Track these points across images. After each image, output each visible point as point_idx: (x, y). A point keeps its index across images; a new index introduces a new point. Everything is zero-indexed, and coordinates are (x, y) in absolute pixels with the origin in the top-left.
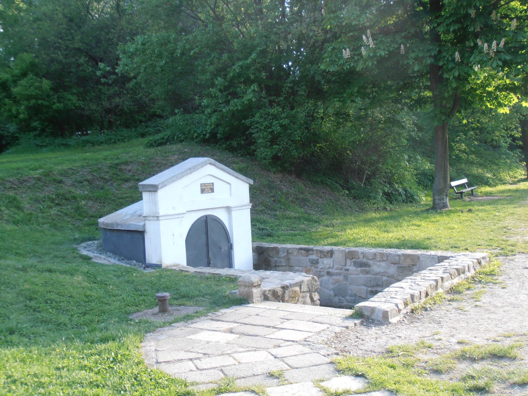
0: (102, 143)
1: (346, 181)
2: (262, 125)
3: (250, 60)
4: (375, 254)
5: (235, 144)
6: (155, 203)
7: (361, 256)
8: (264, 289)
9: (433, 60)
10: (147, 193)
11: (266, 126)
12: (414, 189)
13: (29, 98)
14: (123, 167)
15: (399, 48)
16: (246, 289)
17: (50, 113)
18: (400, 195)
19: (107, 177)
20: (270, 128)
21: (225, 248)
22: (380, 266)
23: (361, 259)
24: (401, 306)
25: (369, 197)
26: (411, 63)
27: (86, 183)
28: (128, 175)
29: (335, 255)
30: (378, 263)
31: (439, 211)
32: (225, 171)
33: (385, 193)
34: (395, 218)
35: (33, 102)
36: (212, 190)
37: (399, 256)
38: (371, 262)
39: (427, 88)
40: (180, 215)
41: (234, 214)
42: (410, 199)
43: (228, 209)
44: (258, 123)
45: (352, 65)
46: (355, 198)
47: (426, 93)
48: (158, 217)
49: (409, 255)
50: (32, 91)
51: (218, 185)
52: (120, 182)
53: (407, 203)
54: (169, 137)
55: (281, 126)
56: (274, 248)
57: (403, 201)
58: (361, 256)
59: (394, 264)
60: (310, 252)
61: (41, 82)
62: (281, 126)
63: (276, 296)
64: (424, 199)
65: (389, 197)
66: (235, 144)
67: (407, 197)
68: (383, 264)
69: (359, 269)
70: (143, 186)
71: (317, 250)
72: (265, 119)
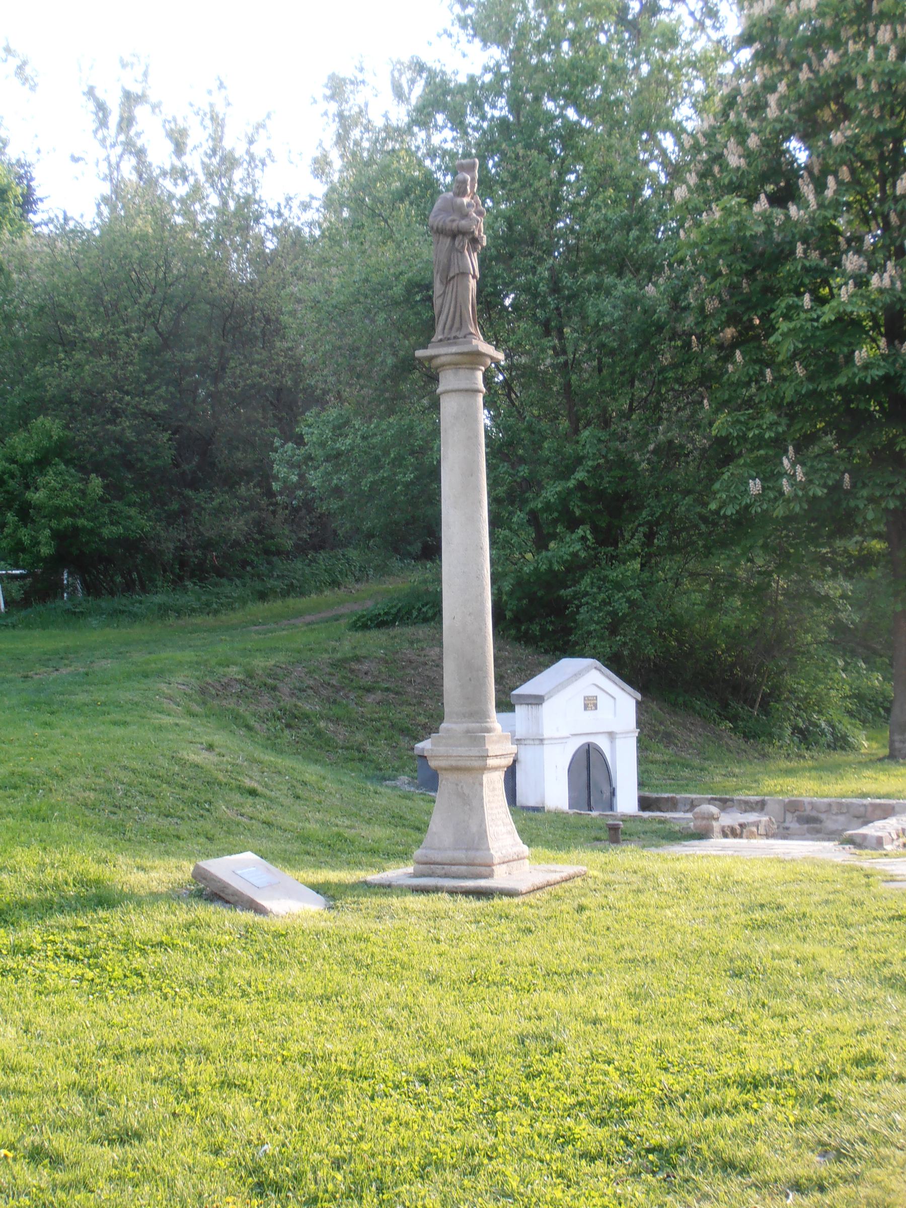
0: (193, 610)
1: (725, 705)
2: (595, 600)
3: (573, 481)
4: (830, 805)
5: (536, 629)
6: (538, 721)
7: (808, 808)
8: (723, 824)
9: (898, 503)
10: (524, 707)
11: (603, 601)
12: (846, 726)
13: (58, 512)
14: (354, 666)
15: (842, 479)
16: (704, 822)
17: (94, 546)
18: (822, 731)
19: (334, 682)
20: (610, 603)
21: (607, 794)
22: (836, 821)
23: (808, 812)
24: (895, 837)
25: (771, 735)
26: (861, 506)
27: (310, 692)
28: (367, 681)
29: (769, 807)
30: (834, 817)
31: (901, 761)
32: (610, 679)
33: (796, 729)
34: (835, 769)
35: (67, 521)
36: (596, 707)
37: (865, 805)
38: (823, 816)
39: (878, 536)
40: (563, 739)
41: (619, 742)
42: (841, 743)
43: (611, 735)
44: (586, 594)
45: (765, 506)
46: (746, 737)
47: (878, 546)
48: (542, 740)
49: (880, 805)
50: (66, 500)
51: (602, 700)
52: (360, 692)
53: (835, 749)
54: (399, 611)
55: (629, 600)
56: (668, 799)
57: (829, 746)
58: (808, 808)
59: (858, 817)
60: (729, 803)
61: (86, 481)
62: (629, 600)
63: (732, 832)
64: (866, 744)
65: (806, 737)
66: (536, 629)
67: (836, 739)
68: (841, 818)
69: (806, 826)
70: (519, 696)
71: (740, 800)
72: (599, 588)
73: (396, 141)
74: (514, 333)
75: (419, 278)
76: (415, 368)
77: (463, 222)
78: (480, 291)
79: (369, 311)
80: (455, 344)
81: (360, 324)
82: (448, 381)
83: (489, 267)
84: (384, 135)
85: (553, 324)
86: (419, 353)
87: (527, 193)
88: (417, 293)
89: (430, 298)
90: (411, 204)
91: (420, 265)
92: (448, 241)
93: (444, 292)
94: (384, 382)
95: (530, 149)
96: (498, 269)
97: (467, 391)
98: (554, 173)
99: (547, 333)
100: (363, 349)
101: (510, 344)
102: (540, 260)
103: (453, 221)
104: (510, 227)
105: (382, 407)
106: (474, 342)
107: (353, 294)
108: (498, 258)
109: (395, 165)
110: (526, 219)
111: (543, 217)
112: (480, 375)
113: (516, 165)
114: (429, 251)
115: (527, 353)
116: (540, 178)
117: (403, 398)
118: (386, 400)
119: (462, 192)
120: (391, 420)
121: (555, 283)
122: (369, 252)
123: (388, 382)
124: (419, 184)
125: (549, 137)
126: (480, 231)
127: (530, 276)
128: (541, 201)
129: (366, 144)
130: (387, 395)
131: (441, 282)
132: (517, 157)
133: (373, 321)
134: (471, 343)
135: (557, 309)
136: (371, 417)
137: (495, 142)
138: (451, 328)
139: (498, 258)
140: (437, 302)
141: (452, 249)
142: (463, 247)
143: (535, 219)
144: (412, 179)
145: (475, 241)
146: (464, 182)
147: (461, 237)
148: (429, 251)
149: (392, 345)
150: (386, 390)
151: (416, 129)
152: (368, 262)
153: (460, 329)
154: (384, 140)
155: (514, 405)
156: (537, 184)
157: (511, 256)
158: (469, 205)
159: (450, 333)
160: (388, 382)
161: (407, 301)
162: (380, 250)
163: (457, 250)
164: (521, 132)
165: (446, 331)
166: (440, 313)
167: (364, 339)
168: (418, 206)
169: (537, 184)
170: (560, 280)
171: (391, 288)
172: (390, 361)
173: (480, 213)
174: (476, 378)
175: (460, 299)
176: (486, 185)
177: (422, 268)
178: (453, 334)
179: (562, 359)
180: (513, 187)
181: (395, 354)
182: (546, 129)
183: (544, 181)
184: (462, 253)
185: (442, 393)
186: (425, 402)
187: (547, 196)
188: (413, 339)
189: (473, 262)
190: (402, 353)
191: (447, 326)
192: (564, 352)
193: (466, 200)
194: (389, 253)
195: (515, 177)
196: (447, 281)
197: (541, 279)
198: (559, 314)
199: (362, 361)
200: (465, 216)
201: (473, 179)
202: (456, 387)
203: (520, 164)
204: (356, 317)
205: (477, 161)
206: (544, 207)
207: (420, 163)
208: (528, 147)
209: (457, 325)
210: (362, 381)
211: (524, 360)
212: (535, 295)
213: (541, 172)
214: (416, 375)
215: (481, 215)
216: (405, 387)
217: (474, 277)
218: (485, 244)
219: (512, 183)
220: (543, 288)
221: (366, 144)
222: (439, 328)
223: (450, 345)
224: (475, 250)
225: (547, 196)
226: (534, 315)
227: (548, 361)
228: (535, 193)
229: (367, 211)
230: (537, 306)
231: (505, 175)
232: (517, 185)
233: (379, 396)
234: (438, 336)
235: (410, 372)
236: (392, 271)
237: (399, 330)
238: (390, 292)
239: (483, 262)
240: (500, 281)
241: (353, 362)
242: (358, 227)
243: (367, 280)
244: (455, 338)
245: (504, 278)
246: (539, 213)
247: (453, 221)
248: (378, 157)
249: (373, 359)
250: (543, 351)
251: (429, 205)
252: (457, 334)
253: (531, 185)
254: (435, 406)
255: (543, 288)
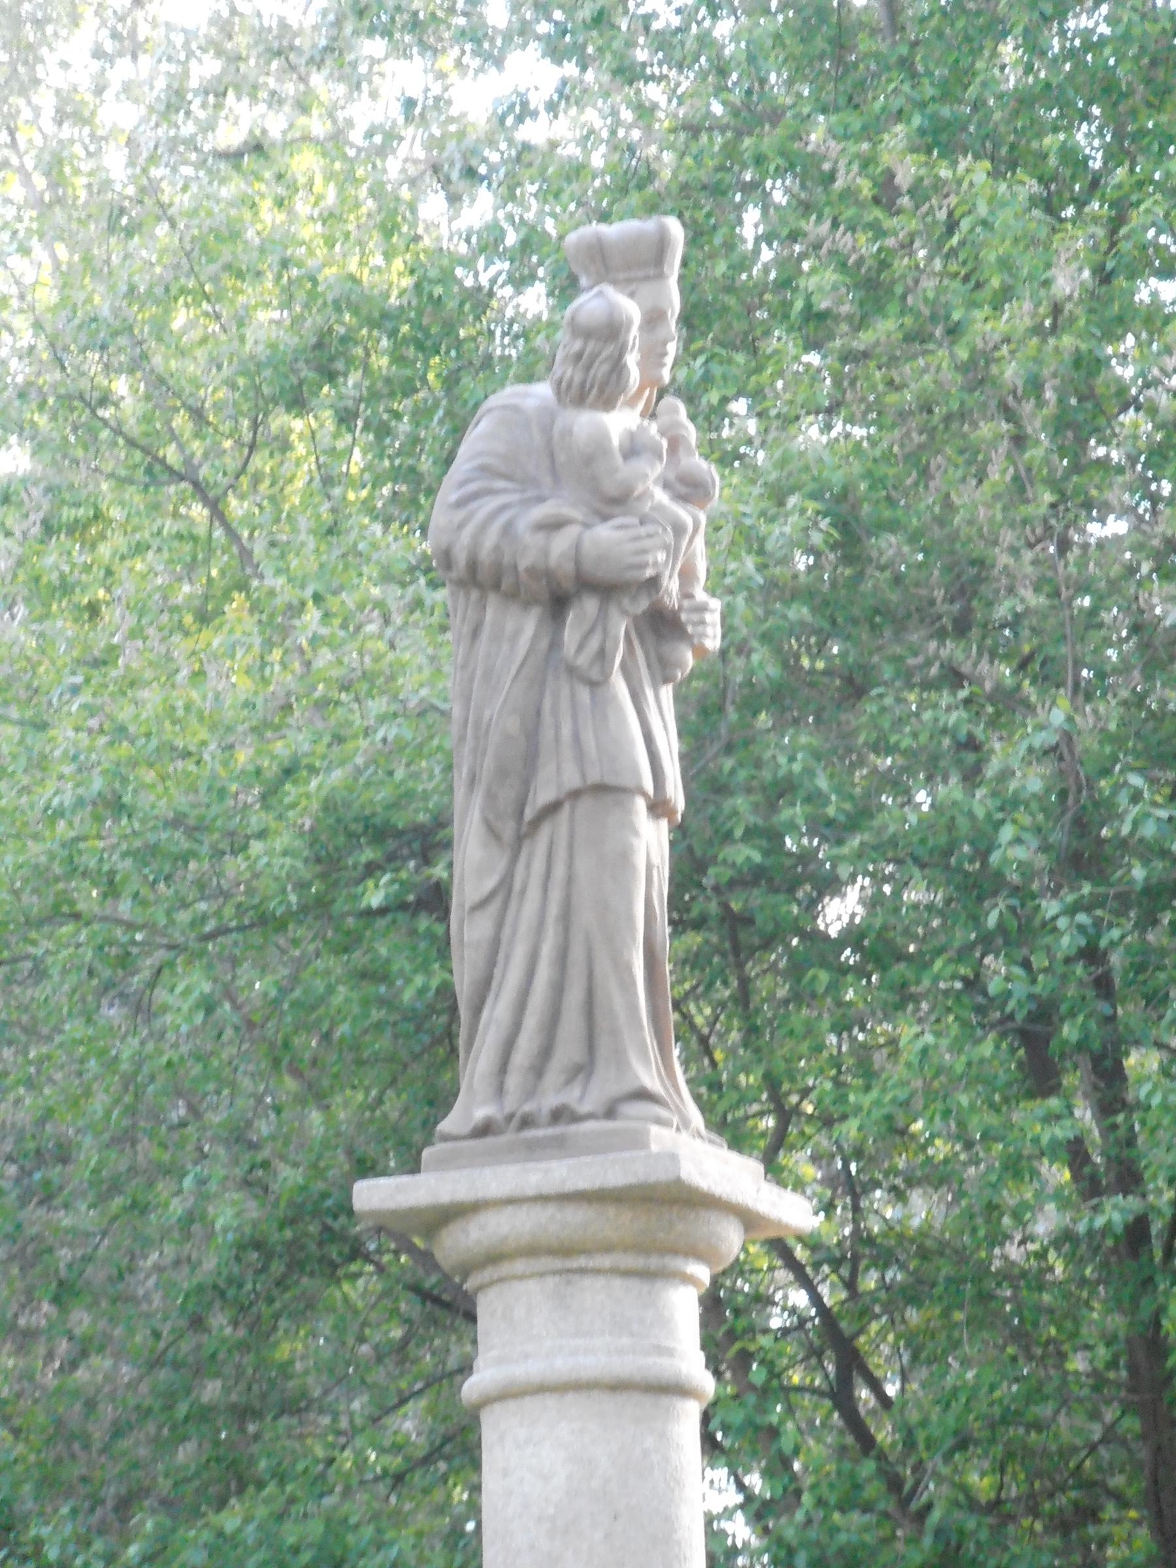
73: (276, 100)
74: (868, 1074)
75: (382, 795)
76: (356, 1252)
77: (605, 533)
78: (689, 866)
79: (125, 961)
80: (560, 1147)
81: (74, 1028)
82: (518, 1337)
83: (740, 743)
84: (208, 68)
85: (1069, 1032)
86: (373, 1195)
87: (935, 370)
88: (371, 869)
89: (437, 899)
90: (346, 418)
91: (388, 731)
92: (527, 625)
93: (505, 885)
94: (197, 1323)
95: (950, 151)
96: (790, 750)
97: (618, 1387)
98: (1069, 280)
99: (1041, 1076)
100: (89, 1153)
101: (850, 1129)
102: (1007, 706)
103: (554, 525)
104: (850, 539)
105: (185, 1454)
106: (660, 1138)
107: (40, 875)
108: (784, 697)
109: (269, 215)
110: (929, 500)
111: (1020, 487)
112: (683, 1307)
113: (879, 232)
114: (430, 667)
115: (937, 1177)
116: (1006, 294)
117: (296, 1406)
118: (204, 1415)
119: (598, 387)
120: (230, 1520)
121: (1082, 826)
122: (130, 660)
123: (219, 1321)
124: (384, 320)
125: (1047, 93)
126: (687, 576)
127: (952, 789)
128: (1009, 414)
129: (119, 114)
130: (211, 1390)
131: (492, 831)
132: (886, 193)
133: (142, 1009)
134: (638, 1141)
135: (1091, 954)
136: (124, 1506)
137: (775, 116)
138: (538, 1069)
139: (784, 697)
140: (470, 932)
141: (548, 661)
142: (603, 656)
143: (976, 503)
144: (351, 298)
145: (662, 625)
146: (611, 331)
147: (590, 605)
148: (430, 667)
149: (239, 1137)
150: (202, 1368)
151: (280, 420)
152: (125, 714)
153: (583, 1070)
154: (217, 91)
155: (867, 1443)
156: (985, 328)
157: (856, 686)
158: (633, 449)
159: (530, 1093)
160: (219, 1321)
161: (318, 908)
162: (181, 646)
163: (572, 671)
164: (906, 64)
165: (513, 1081)
166: (484, 987)
167: (99, 1103)
168: (383, 431)
169: (985, 328)
170: (1108, 810)
171: (239, 847)
172: (230, 1214)
173: (690, 490)
174: (664, 1322)
175: (585, 917)
176: (722, 322)
177: (397, 748)
178: (549, 1100)
179: (1115, 1211)
180: (865, 339)
181: (254, 1183)
182: (1033, 46)
183: (1020, 314)
184: (598, 685)
185: (488, 1401)
186: (409, 1424)
187: (1035, 386)
188: (347, 1104)
189: (648, 731)
190: (288, 1176)
191: (522, 1056)
192: (1129, 1178)
193: (619, 422)
194: (231, 669)
195: (873, 287)
196: (520, 827)
197: (1010, 805)
198: (1104, 986)
199: (83, 1216)
200: (615, 502)
201: (654, 319)
202: (562, 1366)
203: (902, 225)
204: (56, 990)
205: (675, 229)
206: (1019, 441)
207: (391, 223)
208: (939, 139)
209: (568, 1050)
210: (82, 1320)
211: (922, 1210)
212: (978, 886)
213: (1005, 264)
214: (359, 1288)
215: (694, 504)
216: (299, 1348)
217: (659, 807)
218: (713, 641)
219: (860, 323)
220: (1015, 850)
221: (119, 114)
222: (478, 1065)
223: (534, 1150)
224: (663, 671)
225: (1035, 386)
226: (974, 984)
227: (1045, 1225)
228: (977, 371)
229: (117, 458)
230: (987, 942)
231: (821, 283)
232: (885, 328)
233: (170, 1400)
234: (472, 1106)
235: (331, 1271)
236: (242, 757)
237: (280, 1057)
238: (235, 866)
239: (702, 721)
240: (795, 812)
241: (35, 1216)
242: (76, 529)
243: (115, 805)
244: (559, 1115)
245: (815, 798)
246: (999, 474)
247: (554, 525)
248: (178, 187)
249: (139, 1208)
250: (1016, 1167)
251: (437, 427)
252: (571, 1097)
253: (954, 331)
254: (458, 1445)
255: (1015, 850)
